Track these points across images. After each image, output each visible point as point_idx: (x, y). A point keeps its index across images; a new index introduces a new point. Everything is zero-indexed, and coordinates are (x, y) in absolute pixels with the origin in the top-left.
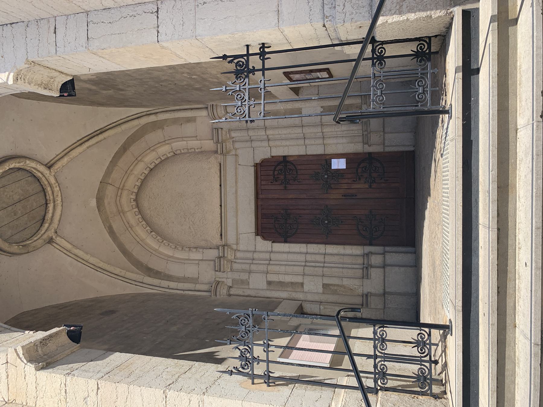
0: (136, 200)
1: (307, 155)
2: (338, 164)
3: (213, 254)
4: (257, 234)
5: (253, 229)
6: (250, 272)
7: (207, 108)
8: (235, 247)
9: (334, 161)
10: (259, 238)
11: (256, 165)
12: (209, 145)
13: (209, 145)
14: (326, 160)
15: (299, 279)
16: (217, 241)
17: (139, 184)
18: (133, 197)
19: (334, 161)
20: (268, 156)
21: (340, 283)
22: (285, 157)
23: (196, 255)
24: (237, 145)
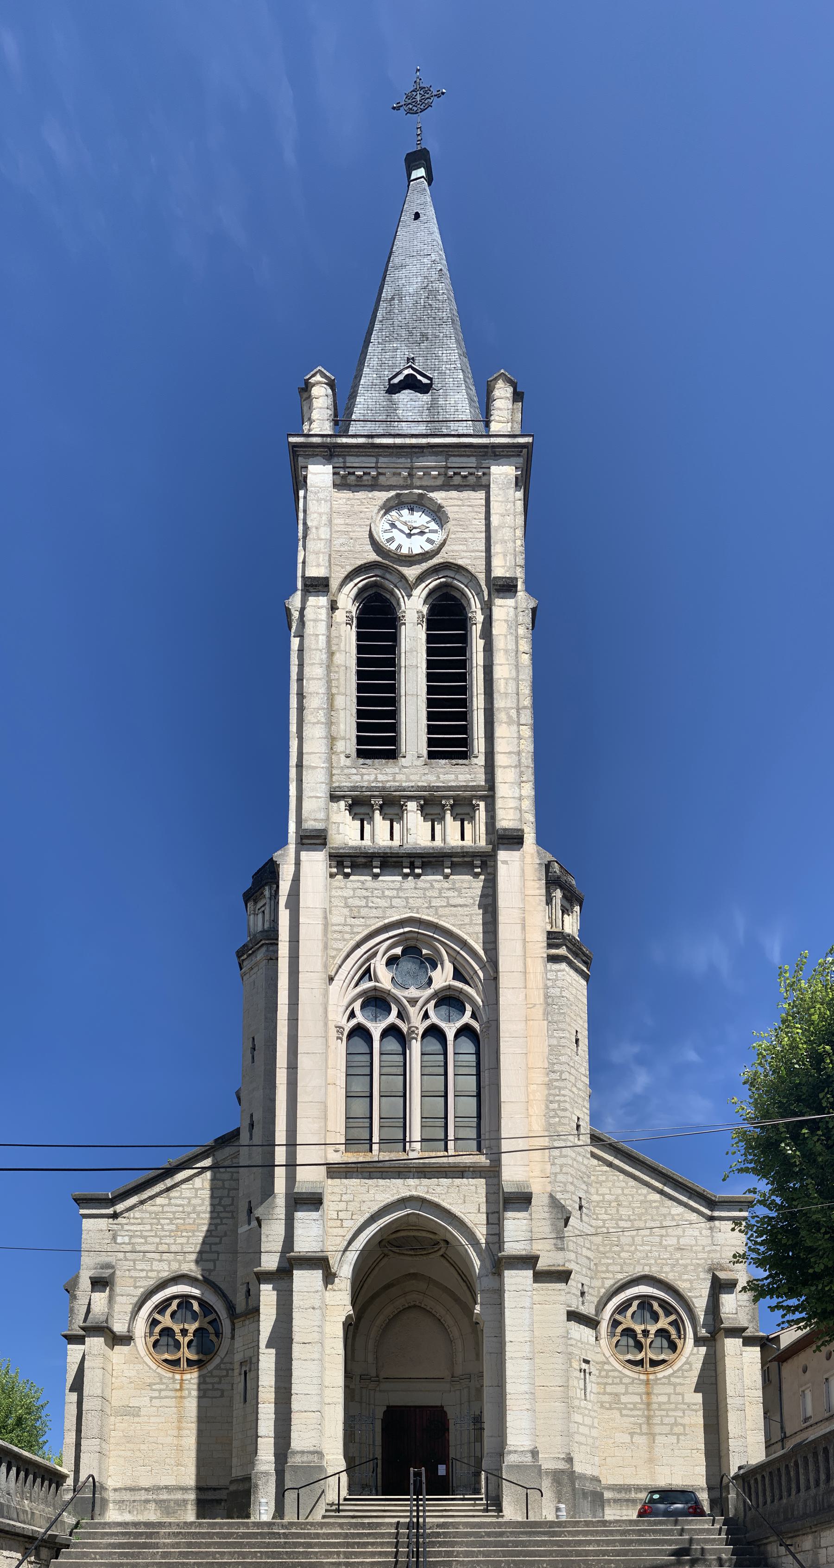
0: (415, 1306)
1: (258, 1403)
2: (442, 1470)
3: (373, 1374)
4: (388, 1407)
5: (391, 1404)
6: (361, 1403)
7: (442, 1256)
8: (378, 1389)
9: (444, 1466)
10: (385, 1408)
11: (442, 1407)
12: (459, 1371)
13: (459, 1371)
14: (445, 1460)
15: (357, 1440)
16: (383, 1375)
17: (428, 1308)
18: (417, 1303)
19: (444, 1466)
20: (449, 1417)
21: (273, 1479)
22: (448, 1429)
23: (371, 1358)
24: (458, 1392)
